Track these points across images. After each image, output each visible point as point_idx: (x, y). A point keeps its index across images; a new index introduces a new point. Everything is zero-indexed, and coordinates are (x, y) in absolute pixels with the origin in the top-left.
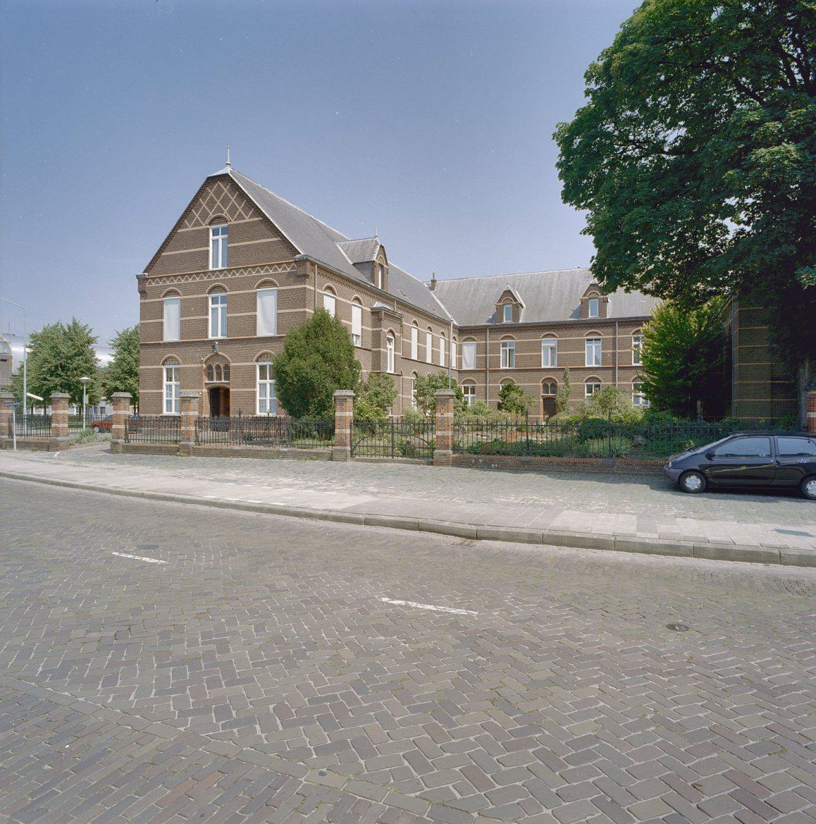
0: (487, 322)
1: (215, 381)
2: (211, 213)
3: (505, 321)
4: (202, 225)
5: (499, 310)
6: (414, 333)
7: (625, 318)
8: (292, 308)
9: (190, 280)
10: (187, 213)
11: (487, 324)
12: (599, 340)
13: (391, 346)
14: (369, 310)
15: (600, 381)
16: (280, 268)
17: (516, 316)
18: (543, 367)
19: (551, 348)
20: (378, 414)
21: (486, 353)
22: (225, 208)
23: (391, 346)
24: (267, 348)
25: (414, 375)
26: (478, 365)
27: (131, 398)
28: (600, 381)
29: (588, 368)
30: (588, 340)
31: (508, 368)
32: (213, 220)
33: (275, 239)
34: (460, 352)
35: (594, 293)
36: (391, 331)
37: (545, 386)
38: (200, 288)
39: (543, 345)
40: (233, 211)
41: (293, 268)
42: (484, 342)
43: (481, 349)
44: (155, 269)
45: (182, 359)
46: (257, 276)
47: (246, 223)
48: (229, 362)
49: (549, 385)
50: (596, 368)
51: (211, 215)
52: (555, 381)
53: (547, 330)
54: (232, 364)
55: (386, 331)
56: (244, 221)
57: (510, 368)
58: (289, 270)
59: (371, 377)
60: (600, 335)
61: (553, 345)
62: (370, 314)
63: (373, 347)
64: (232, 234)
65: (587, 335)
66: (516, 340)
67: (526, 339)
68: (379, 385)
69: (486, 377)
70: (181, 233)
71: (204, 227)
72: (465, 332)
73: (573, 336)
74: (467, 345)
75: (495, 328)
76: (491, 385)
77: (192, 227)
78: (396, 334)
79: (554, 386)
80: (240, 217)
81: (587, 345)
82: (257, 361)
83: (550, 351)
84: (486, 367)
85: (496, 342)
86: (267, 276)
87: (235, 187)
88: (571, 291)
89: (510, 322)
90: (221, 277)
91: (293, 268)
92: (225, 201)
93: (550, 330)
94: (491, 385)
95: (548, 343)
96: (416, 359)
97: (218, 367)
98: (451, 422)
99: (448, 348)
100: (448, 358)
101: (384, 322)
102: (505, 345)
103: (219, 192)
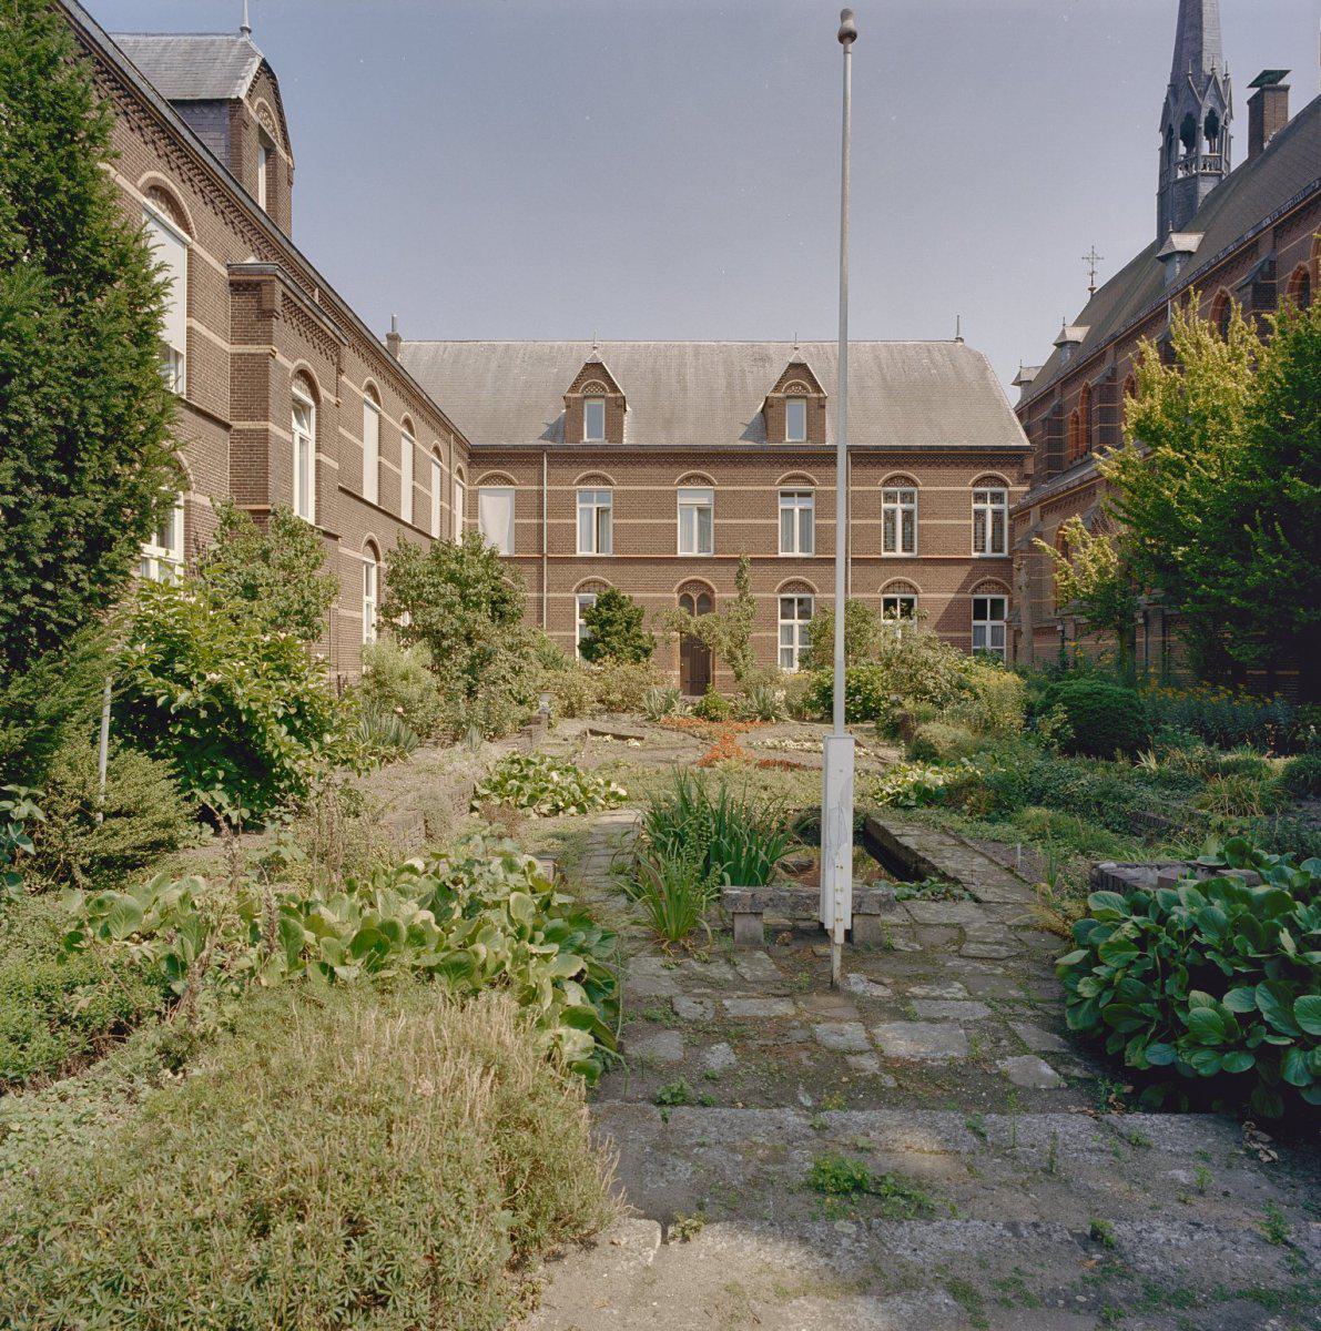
0: (541, 438)
3: (591, 436)
5: (575, 408)
6: (370, 420)
7: (866, 448)
11: (543, 442)
12: (808, 495)
13: (305, 430)
14: (224, 272)
15: (812, 591)
17: (615, 427)
18: (680, 554)
19: (701, 511)
20: (284, 670)
21: (541, 516)
23: (305, 430)
25: (369, 548)
26: (518, 546)
28: (812, 591)
29: (786, 559)
30: (784, 494)
31: (594, 554)
34: (472, 510)
35: (798, 384)
36: (303, 374)
37: (686, 600)
39: (680, 501)
42: (535, 488)
43: (528, 506)
49: (695, 599)
50: (804, 559)
52: (710, 589)
53: (690, 465)
55: (292, 366)
57: (600, 555)
59: (229, 522)
60: (811, 483)
61: (704, 501)
62: (224, 289)
63: (239, 418)
65: (784, 482)
66: (623, 483)
67: (640, 483)
68: (265, 556)
69: (541, 574)
72: (486, 460)
73: (751, 484)
74: (490, 493)
75: (564, 454)
76: (552, 595)
78: (323, 392)
79: (707, 602)
81: (782, 504)
83: (696, 514)
84: (540, 550)
85: (565, 488)
88: (729, 386)
89: (601, 441)
93: (697, 465)
94: (552, 595)
95: (692, 498)
96: (374, 501)
99: (447, 495)
100: (447, 518)
101: (282, 329)
102: (587, 497)
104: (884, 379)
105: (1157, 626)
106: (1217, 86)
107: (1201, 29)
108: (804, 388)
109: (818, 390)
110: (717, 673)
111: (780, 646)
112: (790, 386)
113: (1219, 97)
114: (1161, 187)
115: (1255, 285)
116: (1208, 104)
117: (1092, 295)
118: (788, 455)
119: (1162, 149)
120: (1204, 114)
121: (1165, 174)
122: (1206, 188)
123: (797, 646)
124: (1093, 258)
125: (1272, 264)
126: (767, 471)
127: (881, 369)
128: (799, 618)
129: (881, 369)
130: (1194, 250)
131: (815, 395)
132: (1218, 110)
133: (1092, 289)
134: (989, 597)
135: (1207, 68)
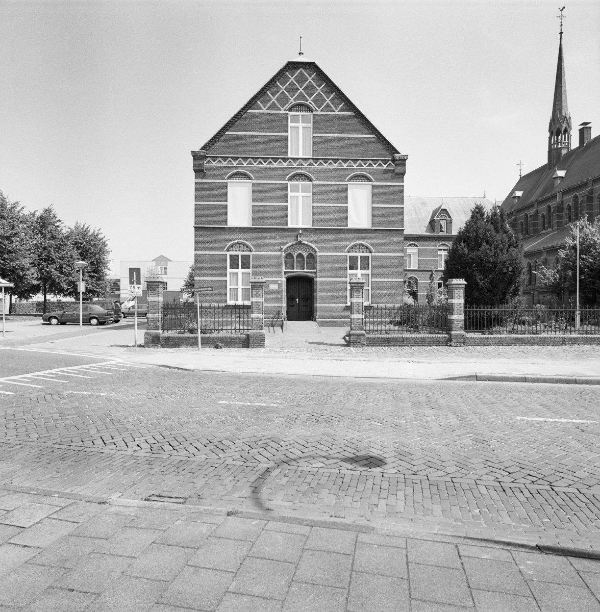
1: (295, 270)
2: (292, 99)
4: (280, 110)
8: (389, 203)
9: (265, 165)
10: (261, 94)
16: (355, 163)
22: (328, 98)
24: (361, 240)
27: (465, 285)
32: (293, 106)
33: (371, 136)
35: (444, 215)
38: (279, 174)
40: (319, 101)
41: (389, 165)
44: (217, 147)
45: (254, 246)
46: (349, 169)
47: (335, 116)
48: (316, 252)
51: (292, 101)
54: (319, 254)
56: (333, 113)
58: (385, 167)
64: (319, 124)
65: (440, 246)
70: (254, 114)
71: (282, 111)
77: (321, 111)
80: (328, 108)
81: (439, 253)
82: (228, 250)
86: (361, 170)
87: (322, 77)
88: (416, 213)
90: (306, 165)
91: (389, 165)
92: (310, 90)
97: (300, 255)
98: (161, 305)
103: (301, 80)
104: (465, 212)
105: (567, 293)
106: (567, 120)
107: (562, 102)
108: (446, 217)
109: (450, 217)
110: (318, 305)
111: (228, 287)
112: (441, 216)
113: (568, 123)
114: (549, 150)
115: (588, 196)
116: (565, 125)
117: (521, 178)
118: (441, 238)
119: (549, 137)
120: (563, 129)
121: (550, 145)
122: (564, 152)
123: (240, 287)
124: (521, 164)
125: (592, 190)
126: (434, 243)
127: (462, 208)
128: (242, 268)
129: (462, 208)
130: (564, 176)
131: (449, 219)
132: (567, 127)
133: (520, 175)
134: (359, 255)
135: (564, 114)
